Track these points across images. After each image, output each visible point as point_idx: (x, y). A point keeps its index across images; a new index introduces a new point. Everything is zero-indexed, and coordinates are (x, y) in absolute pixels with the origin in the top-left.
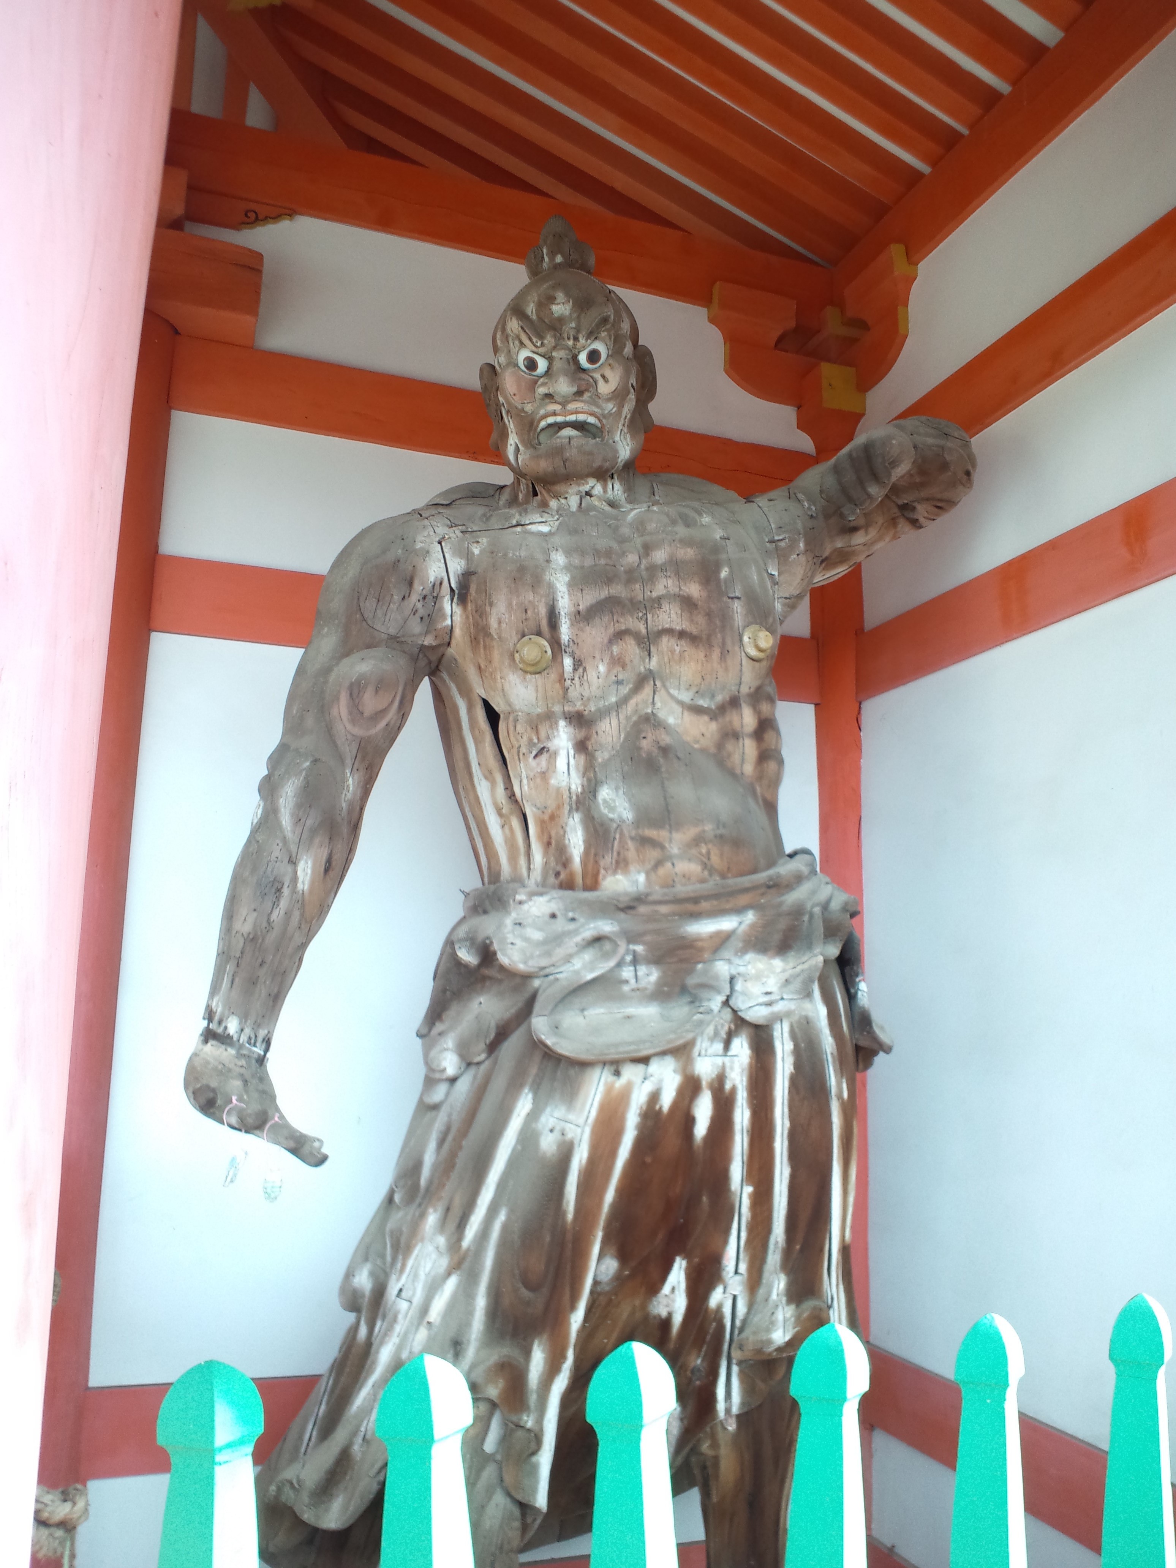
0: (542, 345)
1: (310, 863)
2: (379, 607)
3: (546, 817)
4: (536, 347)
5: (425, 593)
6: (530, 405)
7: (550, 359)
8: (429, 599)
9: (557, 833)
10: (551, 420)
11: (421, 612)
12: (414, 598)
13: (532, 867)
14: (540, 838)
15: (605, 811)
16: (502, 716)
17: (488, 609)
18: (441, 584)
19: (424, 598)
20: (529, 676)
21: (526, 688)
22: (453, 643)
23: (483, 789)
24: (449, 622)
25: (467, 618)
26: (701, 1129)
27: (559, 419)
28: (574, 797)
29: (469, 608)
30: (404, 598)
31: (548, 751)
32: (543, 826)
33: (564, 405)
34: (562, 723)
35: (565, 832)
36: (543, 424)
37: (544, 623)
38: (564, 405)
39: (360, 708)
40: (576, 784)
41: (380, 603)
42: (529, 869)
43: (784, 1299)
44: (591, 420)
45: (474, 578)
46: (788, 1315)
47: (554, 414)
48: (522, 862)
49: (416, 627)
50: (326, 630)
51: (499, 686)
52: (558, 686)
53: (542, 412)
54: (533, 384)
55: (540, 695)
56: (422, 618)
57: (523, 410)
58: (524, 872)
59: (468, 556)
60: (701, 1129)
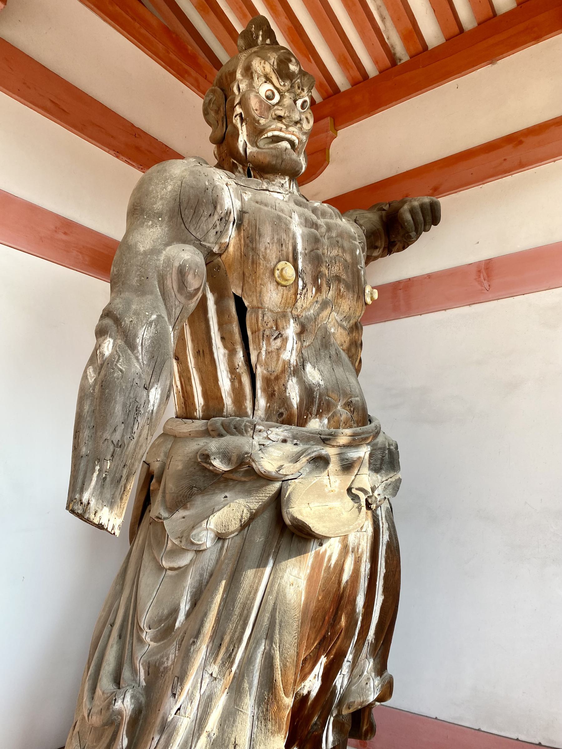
0: (284, 85)
1: (159, 391)
2: (194, 217)
3: (273, 378)
4: (281, 85)
5: (222, 215)
6: (264, 119)
7: (282, 96)
8: (224, 220)
9: (279, 389)
10: (276, 133)
11: (218, 228)
12: (216, 217)
13: (256, 408)
14: (264, 390)
15: (310, 378)
16: (249, 309)
17: (257, 238)
18: (230, 213)
19: (221, 220)
20: (280, 287)
21: (277, 294)
22: (224, 256)
23: (220, 352)
24: (227, 240)
25: (240, 240)
26: (346, 577)
27: (282, 134)
28: (292, 369)
29: (242, 234)
30: (210, 215)
31: (282, 336)
32: (268, 381)
33: (287, 126)
34: (292, 321)
35: (286, 388)
36: (270, 134)
37: (291, 256)
38: (287, 126)
39: (185, 283)
40: (293, 360)
41: (195, 215)
42: (254, 409)
43: (373, 674)
44: (297, 142)
45: (246, 216)
46: (376, 683)
47: (281, 130)
48: (248, 404)
49: (212, 237)
50: (150, 223)
51: (258, 290)
52: (294, 296)
53: (273, 127)
54: (270, 108)
55: (283, 301)
56: (217, 232)
57: (258, 122)
58: (249, 411)
59: (242, 200)
60: (346, 577)
